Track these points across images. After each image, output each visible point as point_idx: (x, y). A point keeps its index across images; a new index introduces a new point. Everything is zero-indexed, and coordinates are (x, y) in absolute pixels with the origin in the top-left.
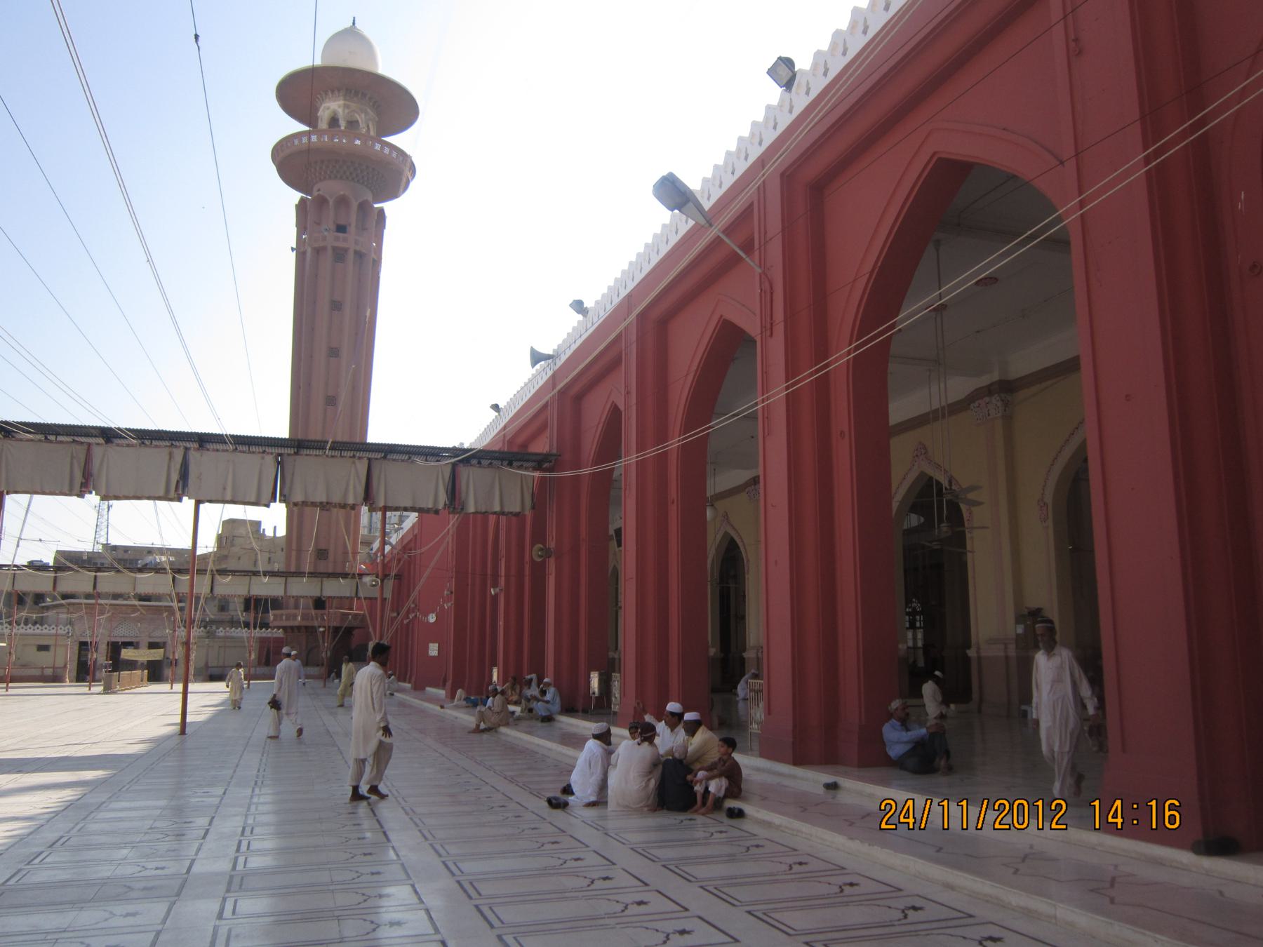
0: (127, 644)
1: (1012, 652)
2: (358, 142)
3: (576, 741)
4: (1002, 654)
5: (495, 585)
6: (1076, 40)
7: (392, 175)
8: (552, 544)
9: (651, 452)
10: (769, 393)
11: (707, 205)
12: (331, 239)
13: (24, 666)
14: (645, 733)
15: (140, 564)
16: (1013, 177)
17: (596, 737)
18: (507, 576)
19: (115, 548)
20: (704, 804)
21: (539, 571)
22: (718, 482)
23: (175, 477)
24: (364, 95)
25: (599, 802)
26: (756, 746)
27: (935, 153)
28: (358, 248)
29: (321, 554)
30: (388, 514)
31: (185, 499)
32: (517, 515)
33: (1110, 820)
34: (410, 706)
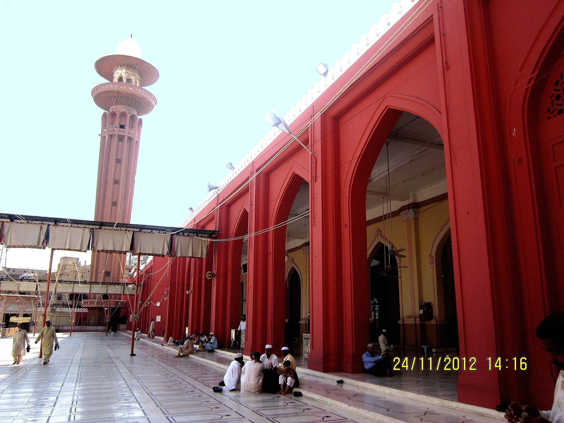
0: (12, 315)
1: (418, 322)
3: (227, 362)
5: (188, 289)
8: (215, 271)
9: (261, 232)
12: (118, 131)
14: (256, 357)
16: (418, 117)
17: (236, 359)
19: (8, 270)
20: (284, 390)
21: (209, 284)
22: (290, 244)
23: (43, 238)
24: (135, 68)
25: (237, 389)
26: (306, 363)
27: (387, 106)
29: (107, 274)
30: (142, 258)
31: (47, 248)
34: (147, 345)
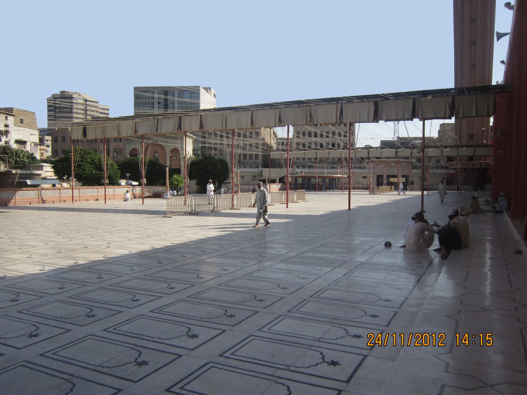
13: (358, 184)
19: (402, 138)
29: (471, 137)
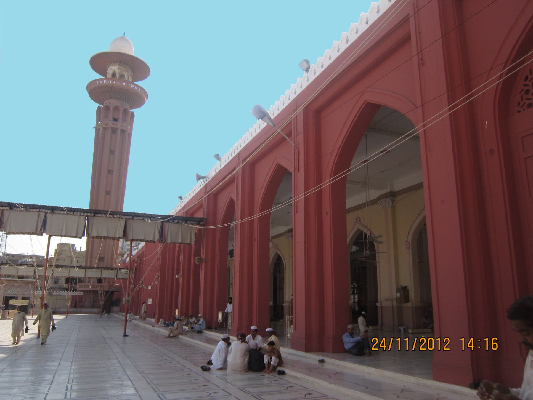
1: (395, 304)
2: (124, 84)
3: (215, 342)
4: (391, 305)
5: (178, 274)
6: (422, 59)
7: (137, 99)
8: (203, 257)
9: (247, 220)
10: (297, 196)
11: (273, 117)
14: (242, 338)
15: (19, 262)
16: (395, 111)
17: (223, 340)
18: (183, 270)
19: (8, 255)
20: (269, 369)
21: (197, 268)
22: (275, 231)
23: (40, 225)
24: (127, 64)
25: (224, 368)
27: (366, 101)
28: (122, 128)
29: (101, 259)
31: (44, 234)
32: (188, 244)
33: (469, 346)
